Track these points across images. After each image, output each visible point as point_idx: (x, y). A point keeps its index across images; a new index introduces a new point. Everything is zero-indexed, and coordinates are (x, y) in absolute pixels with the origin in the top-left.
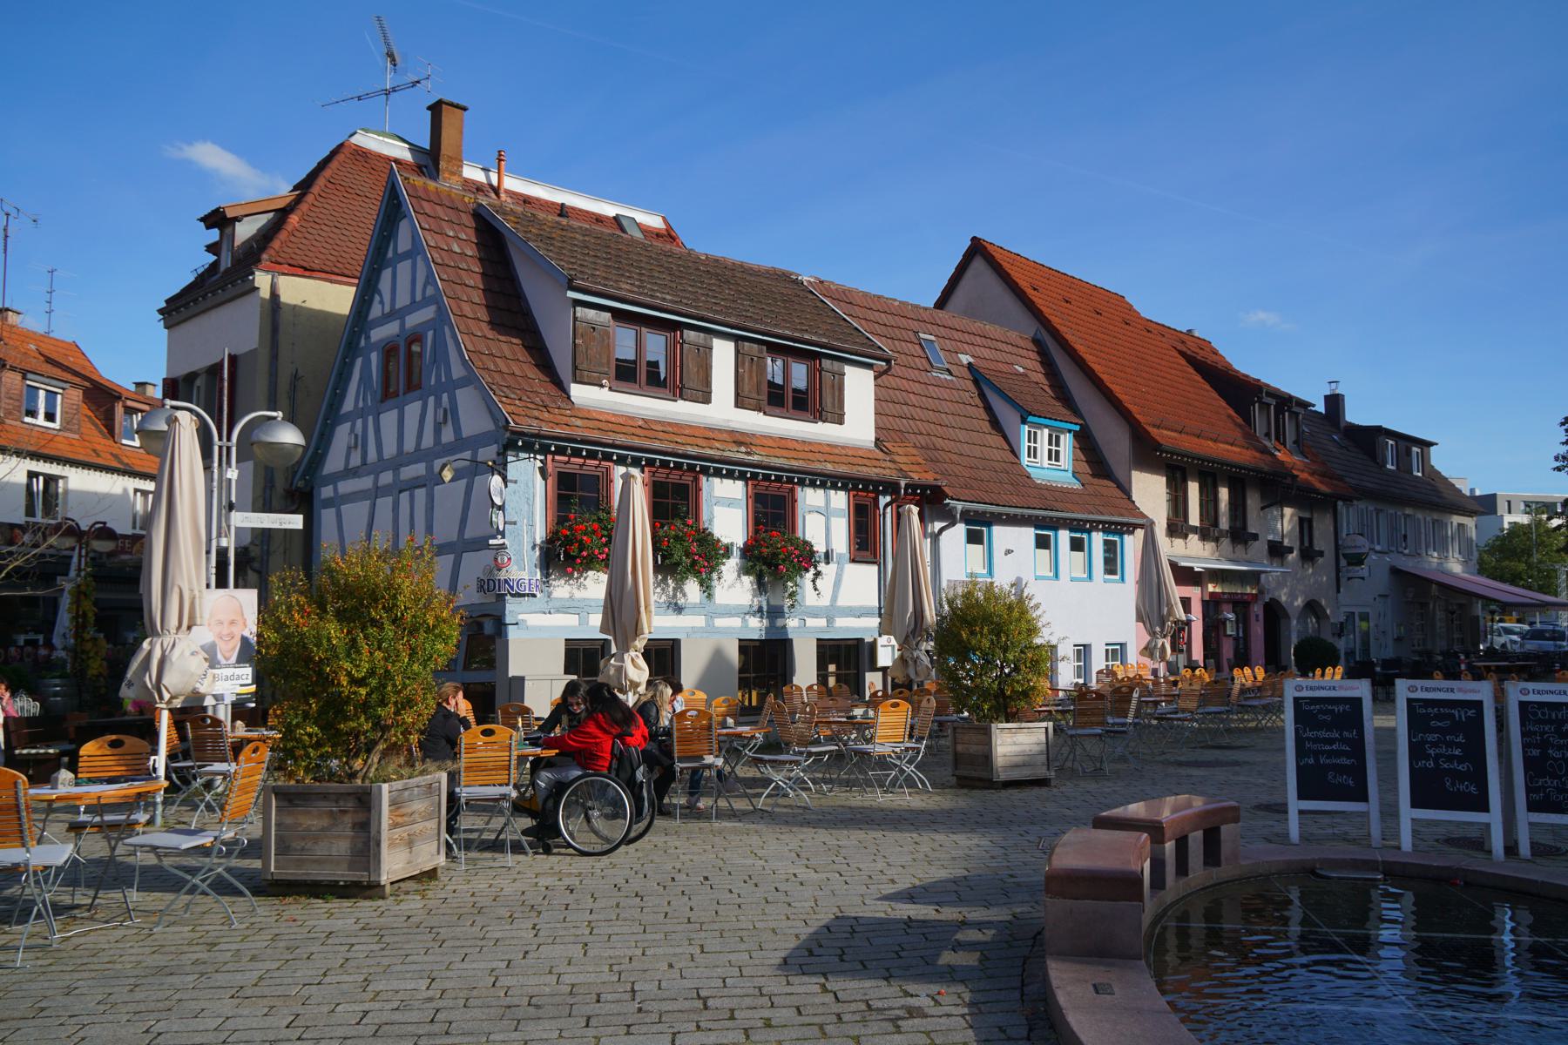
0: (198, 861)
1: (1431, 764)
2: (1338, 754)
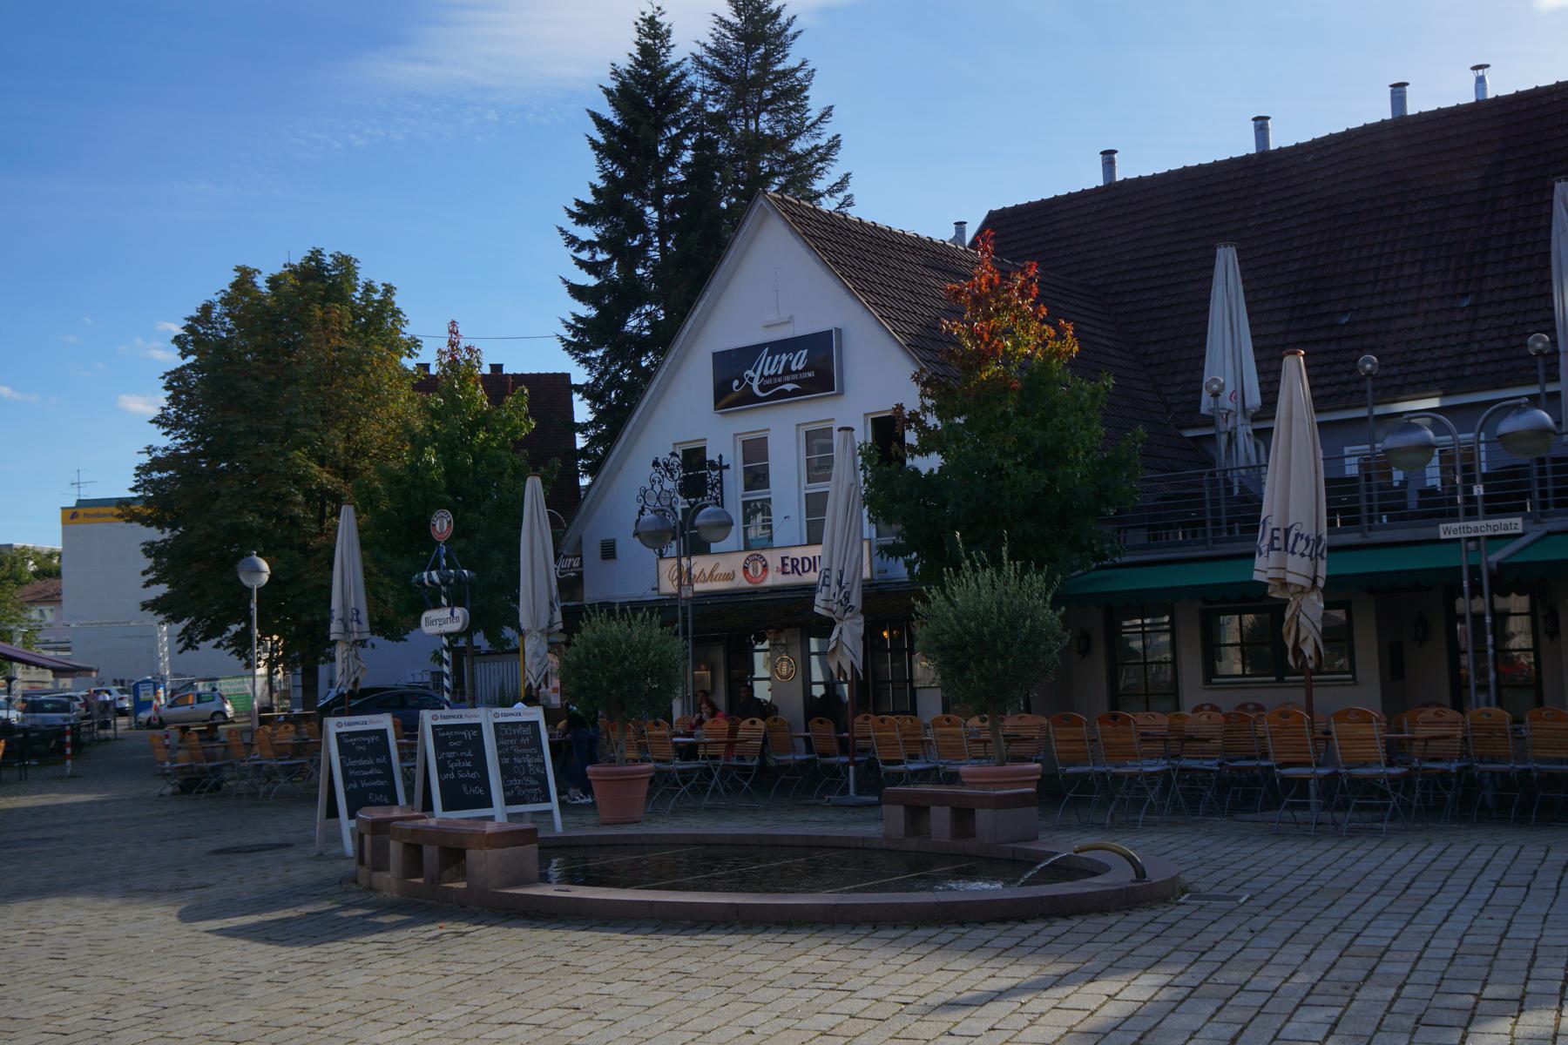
0: (1093, 884)
1: (452, 776)
2: (374, 777)
